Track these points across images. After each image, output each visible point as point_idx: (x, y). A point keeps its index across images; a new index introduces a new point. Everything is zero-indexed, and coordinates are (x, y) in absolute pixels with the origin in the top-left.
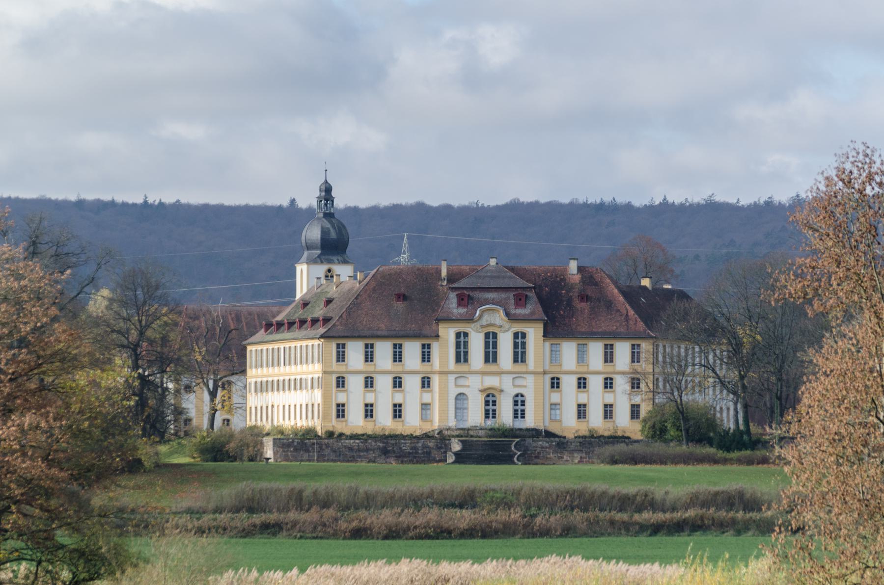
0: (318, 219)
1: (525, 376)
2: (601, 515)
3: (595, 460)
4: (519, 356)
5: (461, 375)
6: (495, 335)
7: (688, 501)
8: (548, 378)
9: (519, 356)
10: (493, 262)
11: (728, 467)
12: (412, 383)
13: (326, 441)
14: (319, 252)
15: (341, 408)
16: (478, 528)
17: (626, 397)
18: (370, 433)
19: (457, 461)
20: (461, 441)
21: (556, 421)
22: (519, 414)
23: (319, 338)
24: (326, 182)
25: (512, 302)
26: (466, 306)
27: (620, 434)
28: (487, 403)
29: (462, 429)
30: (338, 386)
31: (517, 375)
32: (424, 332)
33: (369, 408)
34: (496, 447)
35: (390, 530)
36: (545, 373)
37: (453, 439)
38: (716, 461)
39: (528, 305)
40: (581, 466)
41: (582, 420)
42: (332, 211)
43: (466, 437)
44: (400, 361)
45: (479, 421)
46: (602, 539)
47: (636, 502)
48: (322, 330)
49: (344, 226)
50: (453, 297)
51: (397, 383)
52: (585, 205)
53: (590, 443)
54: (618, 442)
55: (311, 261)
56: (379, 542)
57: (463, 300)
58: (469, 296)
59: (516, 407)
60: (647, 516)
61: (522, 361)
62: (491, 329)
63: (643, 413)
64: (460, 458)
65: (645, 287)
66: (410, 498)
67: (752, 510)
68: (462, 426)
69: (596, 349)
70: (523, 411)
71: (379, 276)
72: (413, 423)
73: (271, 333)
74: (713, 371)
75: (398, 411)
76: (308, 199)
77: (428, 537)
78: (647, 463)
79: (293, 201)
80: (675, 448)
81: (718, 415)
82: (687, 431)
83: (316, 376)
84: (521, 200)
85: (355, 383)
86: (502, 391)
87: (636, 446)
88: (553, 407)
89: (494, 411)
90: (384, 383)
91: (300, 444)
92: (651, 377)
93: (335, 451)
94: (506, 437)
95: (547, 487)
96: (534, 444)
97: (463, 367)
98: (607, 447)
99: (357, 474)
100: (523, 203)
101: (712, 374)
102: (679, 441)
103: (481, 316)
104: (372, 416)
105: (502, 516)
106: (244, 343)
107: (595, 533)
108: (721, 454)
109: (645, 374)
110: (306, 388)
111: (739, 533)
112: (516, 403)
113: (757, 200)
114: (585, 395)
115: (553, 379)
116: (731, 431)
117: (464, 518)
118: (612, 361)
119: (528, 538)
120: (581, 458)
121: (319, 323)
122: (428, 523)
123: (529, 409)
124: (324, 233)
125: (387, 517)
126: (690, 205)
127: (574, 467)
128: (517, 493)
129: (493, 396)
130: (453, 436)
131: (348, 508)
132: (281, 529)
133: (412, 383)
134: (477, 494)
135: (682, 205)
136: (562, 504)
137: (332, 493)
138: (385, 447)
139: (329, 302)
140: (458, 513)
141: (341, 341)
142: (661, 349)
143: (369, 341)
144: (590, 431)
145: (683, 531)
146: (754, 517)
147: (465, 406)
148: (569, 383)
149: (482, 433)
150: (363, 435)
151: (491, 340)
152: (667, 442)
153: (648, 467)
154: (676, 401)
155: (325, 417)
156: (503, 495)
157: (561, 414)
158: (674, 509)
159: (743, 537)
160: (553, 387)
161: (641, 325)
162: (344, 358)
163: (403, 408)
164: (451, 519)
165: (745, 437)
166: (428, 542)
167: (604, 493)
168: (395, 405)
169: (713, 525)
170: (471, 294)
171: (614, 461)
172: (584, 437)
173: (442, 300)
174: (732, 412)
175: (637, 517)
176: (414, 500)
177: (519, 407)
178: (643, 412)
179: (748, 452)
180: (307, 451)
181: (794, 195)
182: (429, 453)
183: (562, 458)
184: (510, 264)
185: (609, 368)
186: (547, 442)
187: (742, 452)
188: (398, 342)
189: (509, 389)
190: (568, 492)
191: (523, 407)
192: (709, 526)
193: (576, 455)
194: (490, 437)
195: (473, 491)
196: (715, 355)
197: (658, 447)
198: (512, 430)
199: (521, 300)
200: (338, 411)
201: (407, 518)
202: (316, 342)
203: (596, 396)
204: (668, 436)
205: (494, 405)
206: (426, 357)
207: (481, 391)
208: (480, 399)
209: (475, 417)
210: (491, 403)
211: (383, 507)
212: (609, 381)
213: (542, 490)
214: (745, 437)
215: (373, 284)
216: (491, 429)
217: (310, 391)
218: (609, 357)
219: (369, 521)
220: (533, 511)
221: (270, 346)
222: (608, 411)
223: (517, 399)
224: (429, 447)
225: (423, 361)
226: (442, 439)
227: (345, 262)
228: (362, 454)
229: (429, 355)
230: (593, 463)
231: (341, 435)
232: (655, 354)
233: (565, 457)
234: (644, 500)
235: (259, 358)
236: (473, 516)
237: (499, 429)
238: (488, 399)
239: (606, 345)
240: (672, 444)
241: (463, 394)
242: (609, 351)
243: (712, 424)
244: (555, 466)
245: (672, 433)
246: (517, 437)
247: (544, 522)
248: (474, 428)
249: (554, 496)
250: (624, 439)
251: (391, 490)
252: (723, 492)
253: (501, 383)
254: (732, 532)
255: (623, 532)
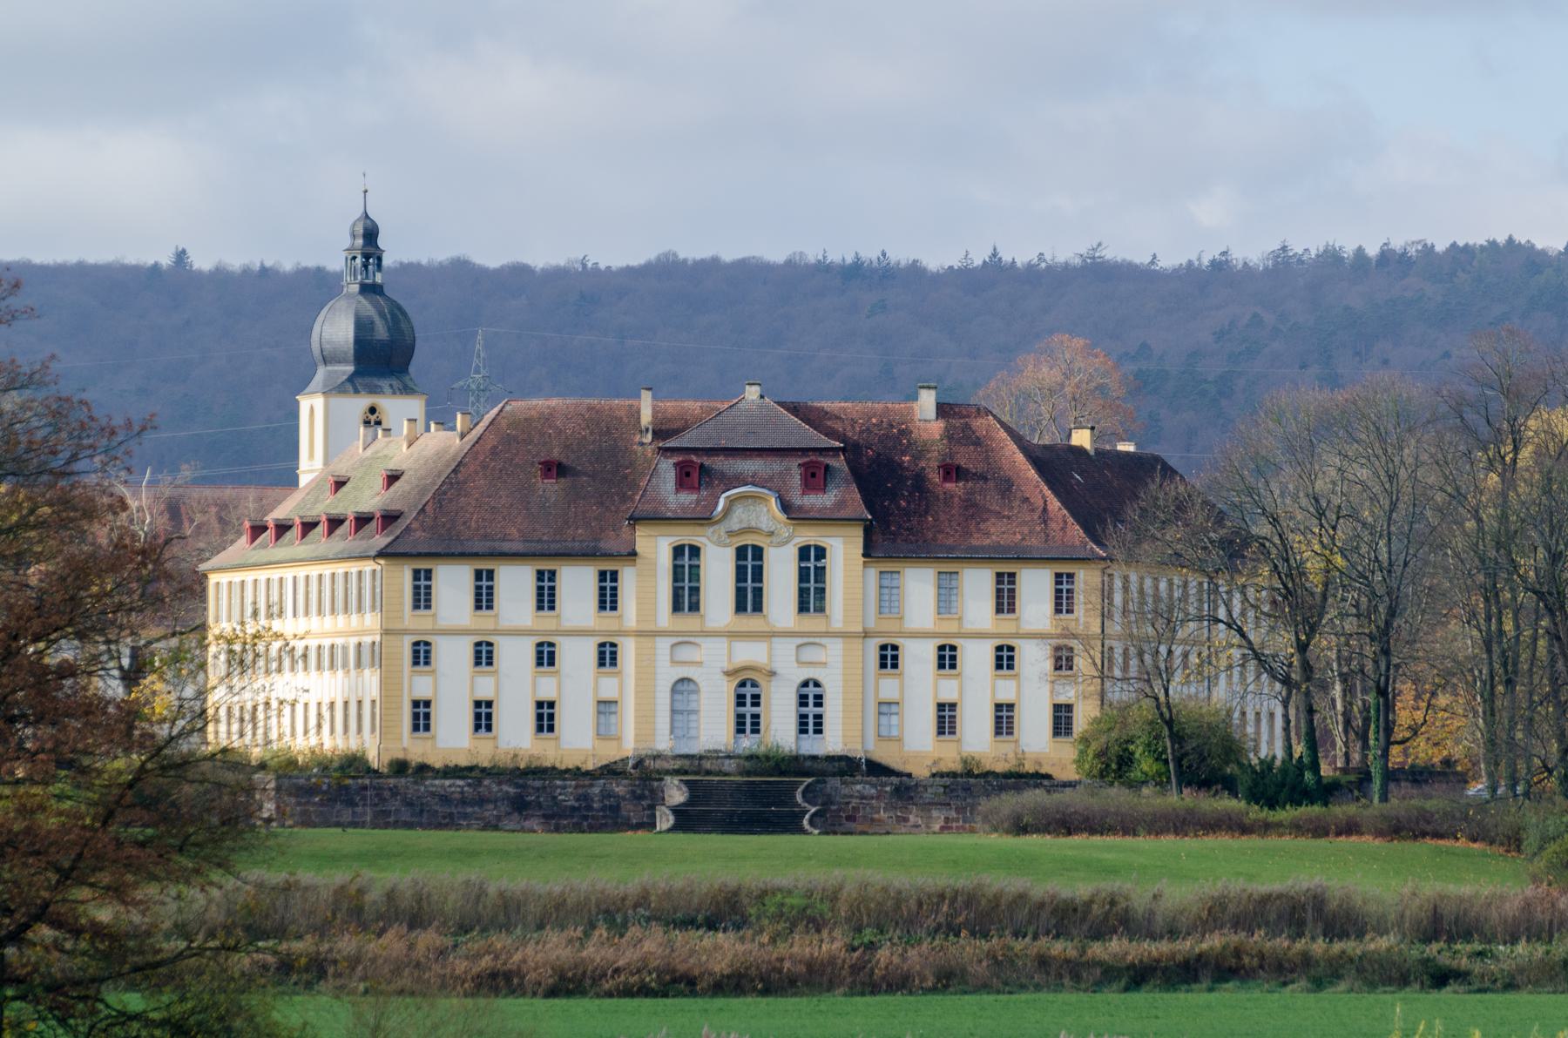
0: (349, 296)
1: (823, 641)
2: (1018, 945)
3: (978, 826)
4: (811, 594)
5: (684, 640)
6: (758, 553)
7: (1204, 914)
8: (873, 646)
9: (811, 594)
10: (752, 393)
11: (1272, 841)
12: (577, 656)
13: (392, 781)
14: (350, 369)
15: (422, 710)
16: (753, 972)
17: (1047, 688)
18: (486, 764)
19: (675, 828)
20: (687, 783)
21: (890, 739)
22: (810, 724)
23: (374, 558)
24: (367, 216)
25: (796, 480)
26: (695, 488)
27: (1029, 768)
28: (740, 700)
29: (687, 757)
30: (416, 663)
31: (808, 639)
32: (602, 545)
33: (546, 711)
34: (762, 794)
35: (562, 977)
36: (866, 635)
37: (668, 779)
38: (1245, 829)
39: (830, 487)
40: (947, 838)
41: (947, 737)
42: (379, 278)
43: (696, 773)
44: (552, 608)
45: (724, 740)
46: (1023, 997)
47: (1090, 917)
48: (381, 541)
49: (404, 313)
50: (667, 470)
51: (546, 656)
52: (823, 269)
53: (967, 789)
54: (1028, 785)
55: (334, 389)
56: (541, 1004)
57: (693, 473)
58: (702, 466)
59: (804, 710)
60: (1115, 948)
61: (690, 609)
62: (749, 540)
63: (1080, 723)
64: (686, 820)
65: (1080, 450)
66: (598, 906)
67: (1344, 935)
68: (685, 751)
69: (978, 583)
70: (819, 717)
71: (504, 423)
72: (576, 742)
73: (264, 546)
74: (1240, 631)
75: (545, 716)
76: (333, 252)
77: (644, 991)
78: (1092, 831)
79: (181, 255)
80: (1150, 799)
81: (1250, 730)
82: (1179, 761)
83: (367, 640)
84: (681, 256)
85: (453, 655)
86: (772, 674)
87: (1066, 796)
88: (885, 709)
89: (756, 717)
90: (515, 655)
91: (340, 791)
92: (1099, 643)
93: (410, 804)
94: (782, 774)
95: (897, 884)
96: (845, 791)
97: (687, 622)
98: (1004, 796)
99: (470, 854)
100: (685, 260)
101: (1236, 640)
102: (1159, 784)
103: (727, 511)
104: (489, 728)
105: (802, 947)
106: (202, 567)
107: (1006, 984)
108: (1256, 813)
109: (1085, 639)
110: (345, 665)
111: (1318, 984)
112: (803, 700)
113: (1194, 258)
114: (1012, 684)
115: (883, 648)
116: (1278, 763)
117: (722, 950)
118: (1012, 610)
119: (863, 994)
120: (947, 819)
121: (373, 524)
122: (644, 959)
123: (833, 712)
124: (362, 327)
125: (553, 949)
126: (1049, 267)
127: (932, 838)
128: (833, 897)
129: (754, 685)
130: (668, 772)
131: (464, 929)
132: (322, 974)
133: (577, 656)
134: (746, 901)
135: (1030, 267)
136: (930, 923)
137: (429, 895)
138: (520, 797)
139: (393, 478)
140: (708, 940)
141: (423, 565)
142: (1118, 583)
143: (485, 565)
144: (965, 762)
145: (1196, 980)
146: (1349, 951)
147: (693, 706)
148: (919, 657)
149: (729, 766)
150: (471, 769)
151: (750, 563)
152: (1134, 785)
153: (1097, 839)
154: (1157, 699)
155: (385, 729)
156: (804, 902)
157: (901, 726)
158: (1173, 933)
159: (1326, 995)
160: (883, 666)
161: (1076, 532)
162: (428, 600)
163: (556, 710)
164: (692, 952)
165: (1308, 776)
166: (648, 1002)
167: (1022, 897)
168: (540, 705)
169: (1261, 967)
170: (707, 461)
171: (1021, 829)
172: (953, 774)
173: (643, 474)
174: (1279, 722)
175: (1097, 950)
176: (607, 911)
177: (811, 710)
178: (1081, 721)
179: (1316, 810)
180: (351, 803)
181: (1276, 246)
182: (615, 809)
183: (906, 820)
184: (790, 398)
185: (1006, 625)
186: (874, 786)
187: (1303, 809)
188: (546, 565)
189: (786, 671)
190: (942, 896)
191: (818, 710)
192: (1253, 970)
193: (935, 813)
194: (748, 773)
195: (736, 893)
196: (1245, 599)
197: (1117, 797)
198: (796, 758)
199: (816, 477)
200: (416, 716)
201: (597, 951)
202: (368, 567)
203: (920, 681)
204: (1135, 774)
205: (756, 704)
206: (608, 599)
207: (728, 674)
208: (728, 690)
209: (714, 730)
210: (748, 700)
211: (541, 927)
212: (889, 653)
213: (885, 889)
214: (1308, 776)
215: (491, 440)
216: (750, 757)
217: (353, 672)
218: (1005, 601)
219: (517, 957)
220: (868, 935)
221: (262, 575)
222: (1004, 718)
223: (805, 691)
224: (617, 796)
225: (602, 607)
226: (642, 777)
227: (407, 390)
228: (469, 810)
229: (490, 594)
230: (973, 831)
231: (423, 769)
232: (1106, 594)
233: (912, 818)
234: (1107, 914)
235: (236, 601)
236: (740, 948)
237: (767, 758)
238: (742, 691)
239: (999, 575)
240: (1145, 791)
241: (689, 680)
242: (1006, 587)
243: (1231, 749)
244: (890, 838)
245: (1145, 767)
246: (807, 775)
247: (896, 960)
248: (713, 755)
249: (913, 903)
250: (1039, 779)
251: (557, 889)
252: (1280, 896)
253: (770, 656)
254: (1303, 983)
255: (1067, 981)
